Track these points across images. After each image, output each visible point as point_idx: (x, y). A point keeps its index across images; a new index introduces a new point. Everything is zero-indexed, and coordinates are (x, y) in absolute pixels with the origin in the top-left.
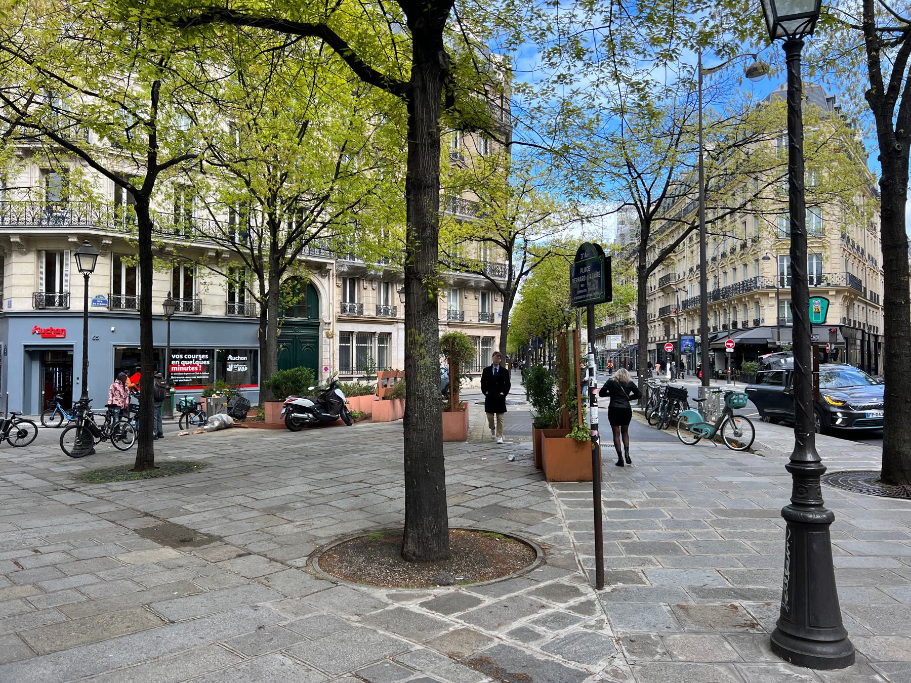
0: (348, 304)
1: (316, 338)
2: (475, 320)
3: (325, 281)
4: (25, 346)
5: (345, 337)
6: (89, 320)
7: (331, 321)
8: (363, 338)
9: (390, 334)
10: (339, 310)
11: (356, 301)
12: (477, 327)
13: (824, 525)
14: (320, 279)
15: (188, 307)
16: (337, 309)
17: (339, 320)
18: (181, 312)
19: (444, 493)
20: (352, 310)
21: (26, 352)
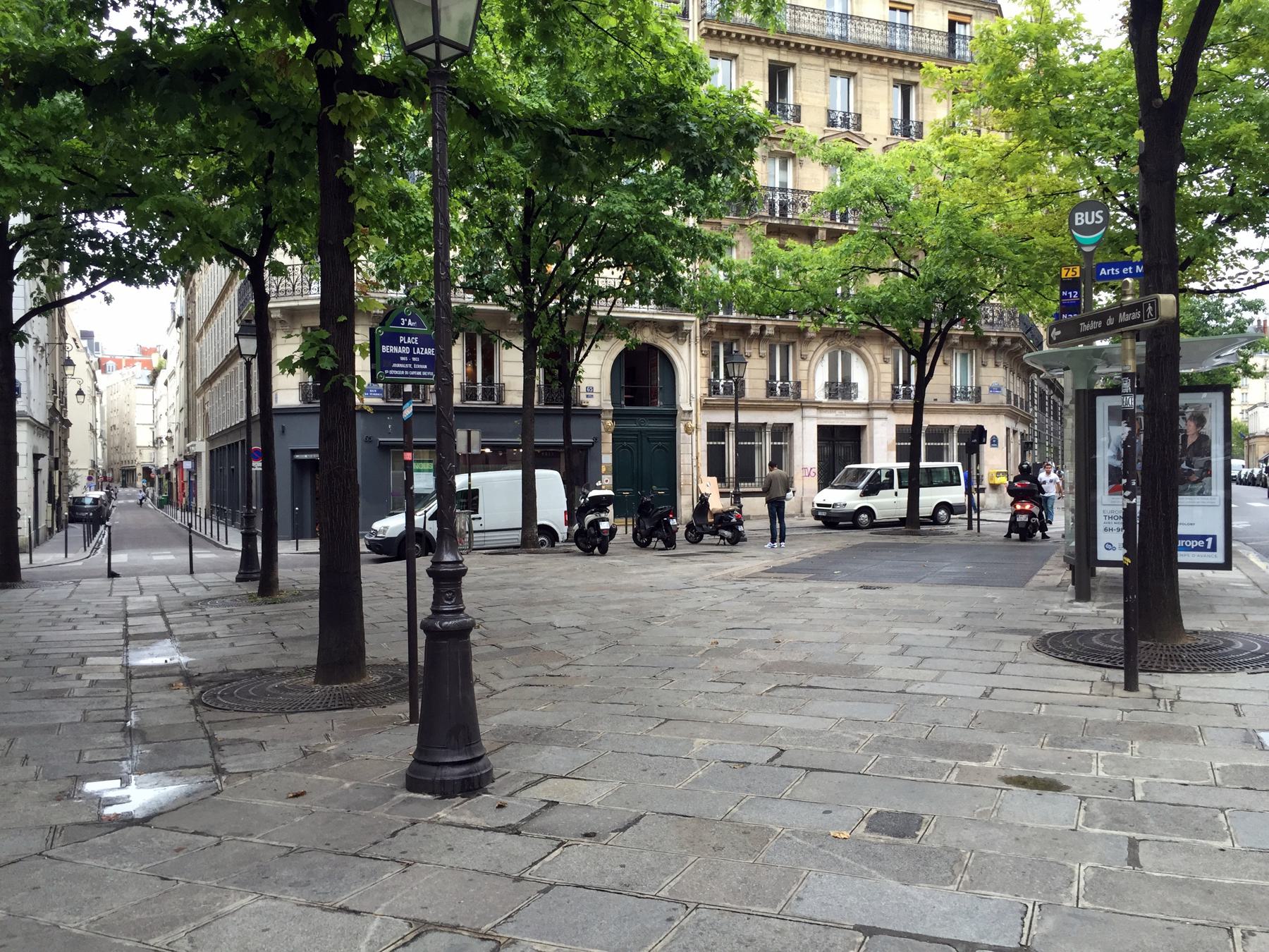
0: (901, 387)
1: (671, 437)
2: (820, 396)
3: (684, 349)
4: (294, 452)
5: (716, 432)
6: (1234, 486)
7: (693, 408)
8: (747, 433)
9: (791, 425)
10: (706, 391)
11: (791, 379)
12: (948, 412)
13: (463, 632)
14: (676, 345)
15: (488, 395)
16: (702, 389)
17: (706, 406)
18: (479, 403)
19: (361, 633)
20: (785, 391)
21: (295, 462)
